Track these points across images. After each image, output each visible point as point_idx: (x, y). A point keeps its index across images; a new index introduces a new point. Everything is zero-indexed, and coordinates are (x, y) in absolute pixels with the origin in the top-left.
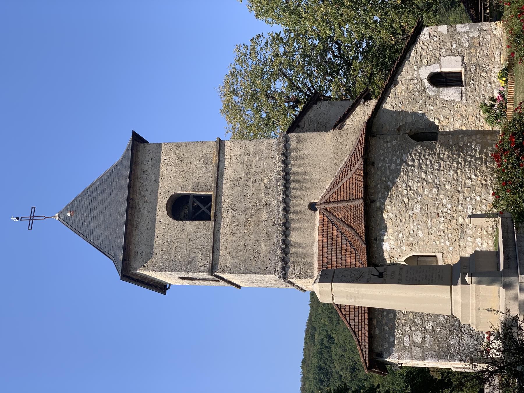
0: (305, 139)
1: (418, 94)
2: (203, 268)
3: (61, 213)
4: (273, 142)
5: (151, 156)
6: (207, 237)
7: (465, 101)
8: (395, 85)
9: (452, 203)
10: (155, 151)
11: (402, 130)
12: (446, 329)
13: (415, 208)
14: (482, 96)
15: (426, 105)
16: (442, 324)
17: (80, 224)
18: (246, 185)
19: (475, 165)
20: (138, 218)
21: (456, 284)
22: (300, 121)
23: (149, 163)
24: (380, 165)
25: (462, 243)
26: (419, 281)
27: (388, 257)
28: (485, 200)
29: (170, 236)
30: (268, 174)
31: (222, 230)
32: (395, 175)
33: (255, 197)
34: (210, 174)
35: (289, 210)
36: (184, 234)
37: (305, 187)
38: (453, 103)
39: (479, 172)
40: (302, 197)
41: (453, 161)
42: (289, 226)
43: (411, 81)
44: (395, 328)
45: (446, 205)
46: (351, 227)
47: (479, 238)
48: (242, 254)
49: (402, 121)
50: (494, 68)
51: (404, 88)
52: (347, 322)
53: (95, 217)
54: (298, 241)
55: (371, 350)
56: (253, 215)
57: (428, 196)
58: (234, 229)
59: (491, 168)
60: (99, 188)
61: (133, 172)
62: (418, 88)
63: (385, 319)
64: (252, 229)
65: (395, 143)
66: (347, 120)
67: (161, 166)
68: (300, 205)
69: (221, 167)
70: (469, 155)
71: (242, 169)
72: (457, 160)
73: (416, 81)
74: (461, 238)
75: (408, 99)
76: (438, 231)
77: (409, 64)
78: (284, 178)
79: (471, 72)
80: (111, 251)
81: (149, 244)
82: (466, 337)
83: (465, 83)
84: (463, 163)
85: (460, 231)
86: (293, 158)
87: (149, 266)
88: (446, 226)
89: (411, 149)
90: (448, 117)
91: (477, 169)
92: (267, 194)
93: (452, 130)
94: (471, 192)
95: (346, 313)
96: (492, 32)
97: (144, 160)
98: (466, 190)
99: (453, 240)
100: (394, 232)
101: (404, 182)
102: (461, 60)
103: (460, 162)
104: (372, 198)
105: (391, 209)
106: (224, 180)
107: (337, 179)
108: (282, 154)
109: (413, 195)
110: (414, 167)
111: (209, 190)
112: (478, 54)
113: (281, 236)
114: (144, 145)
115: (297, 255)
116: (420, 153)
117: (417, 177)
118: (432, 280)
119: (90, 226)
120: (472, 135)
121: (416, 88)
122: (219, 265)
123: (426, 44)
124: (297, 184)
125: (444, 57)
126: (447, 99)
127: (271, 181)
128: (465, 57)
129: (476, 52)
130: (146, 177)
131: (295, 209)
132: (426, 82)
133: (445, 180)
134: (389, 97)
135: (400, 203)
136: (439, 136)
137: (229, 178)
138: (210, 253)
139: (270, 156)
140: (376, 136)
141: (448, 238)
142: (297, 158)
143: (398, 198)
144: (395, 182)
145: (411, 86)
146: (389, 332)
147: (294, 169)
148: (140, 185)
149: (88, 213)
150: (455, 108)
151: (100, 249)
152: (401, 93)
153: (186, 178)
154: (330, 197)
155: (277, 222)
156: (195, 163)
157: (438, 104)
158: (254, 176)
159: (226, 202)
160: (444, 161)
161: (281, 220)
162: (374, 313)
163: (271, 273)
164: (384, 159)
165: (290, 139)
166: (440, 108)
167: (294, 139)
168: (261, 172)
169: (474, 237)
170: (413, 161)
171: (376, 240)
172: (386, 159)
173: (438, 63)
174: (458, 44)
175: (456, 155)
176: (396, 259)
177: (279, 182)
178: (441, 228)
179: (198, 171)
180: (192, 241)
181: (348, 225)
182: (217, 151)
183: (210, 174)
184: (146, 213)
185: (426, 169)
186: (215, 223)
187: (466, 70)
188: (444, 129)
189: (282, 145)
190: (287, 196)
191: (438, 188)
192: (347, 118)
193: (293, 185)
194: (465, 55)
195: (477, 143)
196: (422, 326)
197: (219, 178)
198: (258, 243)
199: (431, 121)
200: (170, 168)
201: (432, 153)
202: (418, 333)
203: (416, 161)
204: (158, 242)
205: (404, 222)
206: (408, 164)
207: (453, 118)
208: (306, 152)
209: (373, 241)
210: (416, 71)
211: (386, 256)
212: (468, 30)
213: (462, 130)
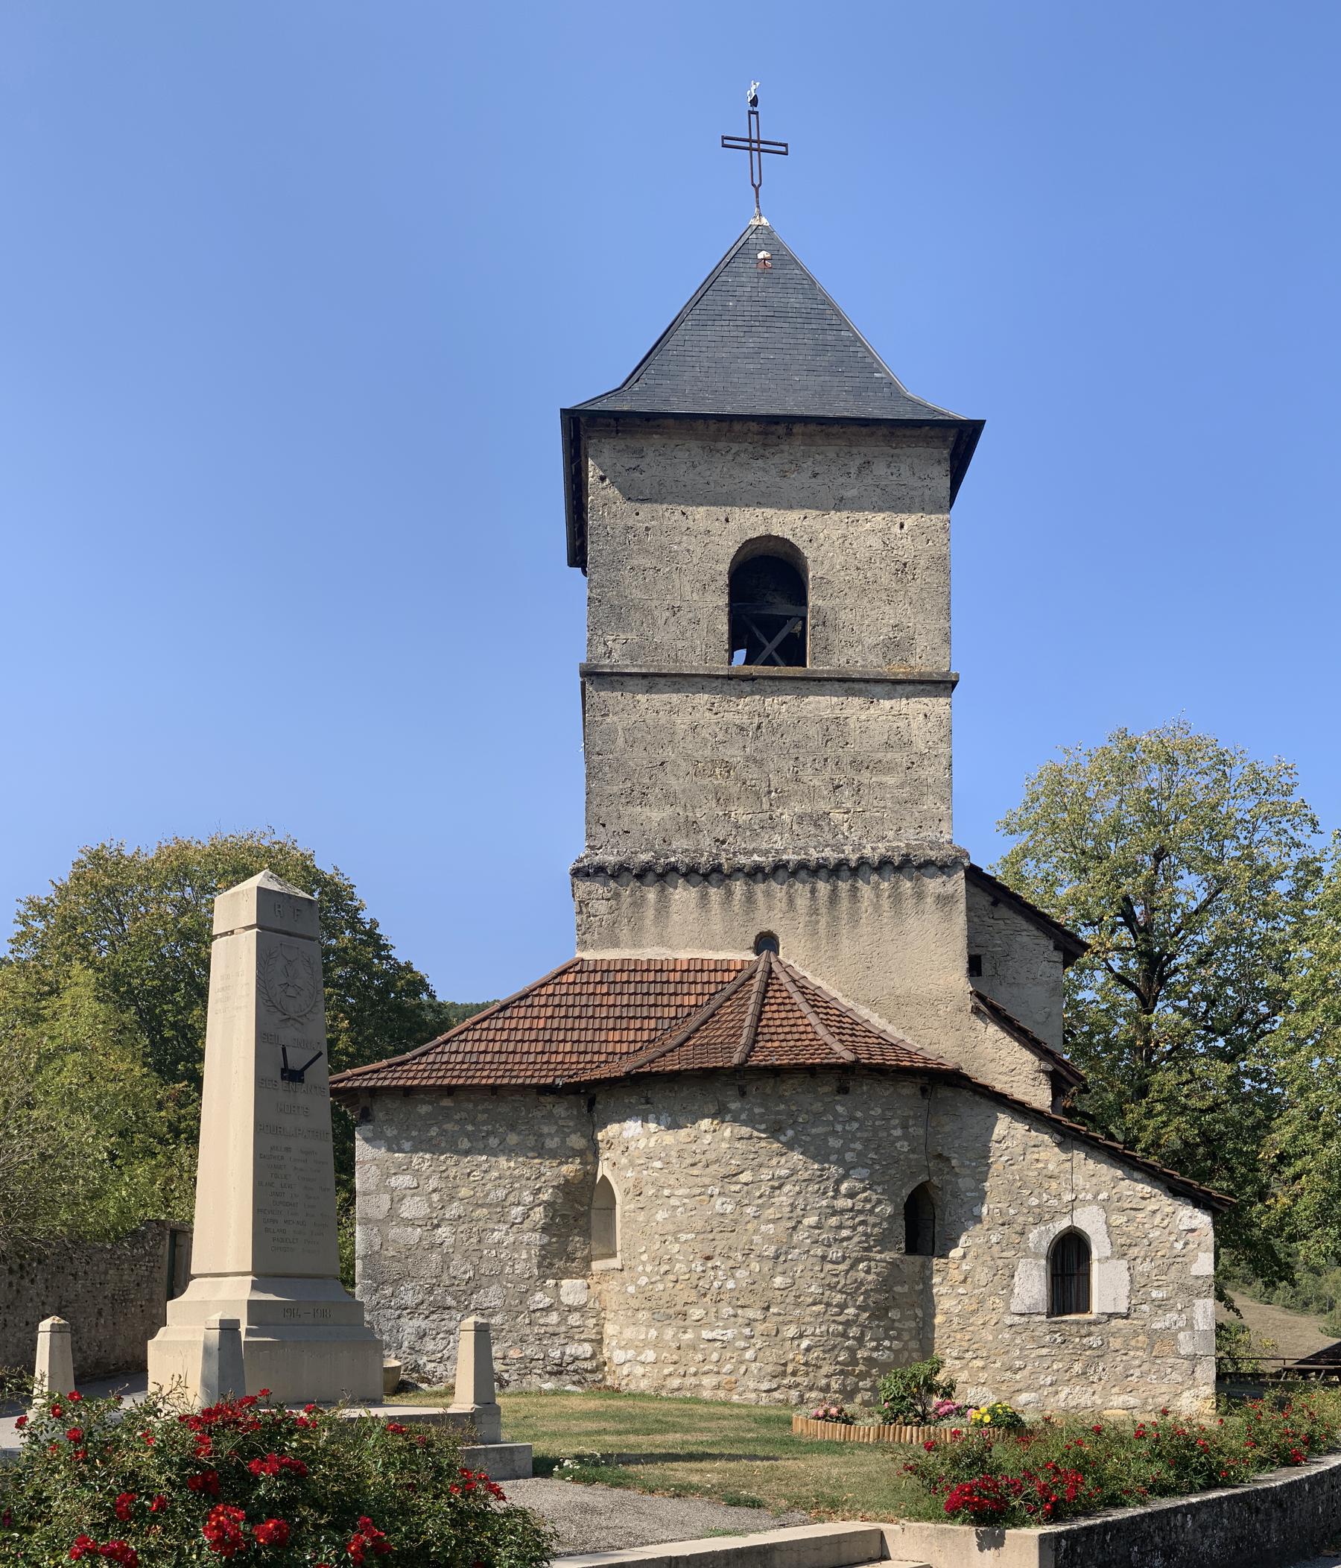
0: (948, 918)
1: (1034, 1204)
2: (601, 649)
3: (769, 231)
5: (914, 482)
6: (683, 658)
7: (1009, 1322)
8: (1059, 1145)
9: (737, 1291)
10: (927, 492)
12: (436, 1277)
15: (1003, 1225)
17: (731, 289)
18: (826, 760)
19: (834, 1347)
20: (737, 454)
21: (255, 1286)
22: (1010, 907)
23: (894, 478)
24: (840, 1109)
25: (644, 1315)
26: (271, 1185)
27: (611, 1134)
29: (688, 551)
31: (703, 698)
32: (812, 1148)
33: (793, 786)
34: (859, 659)
35: (755, 881)
36: (692, 592)
37: (817, 922)
39: (817, 1358)
40: (792, 914)
41: (848, 1294)
42: (714, 882)
44: (434, 1154)
45: (733, 1277)
46: (688, 1039)
48: (637, 758)
49: (962, 1165)
50: (1094, 1393)
51: (1051, 1167)
52: (455, 1036)
53: (746, 329)
54: (674, 908)
55: (373, 1092)
56: (744, 783)
57: (756, 1231)
58: (705, 733)
59: (828, 1385)
60: (830, 337)
61: (864, 430)
62: (1048, 1204)
63: (456, 1128)
64: (706, 781)
66: (996, 1028)
67: (883, 515)
68: (770, 908)
69: (878, 689)
70: (863, 1334)
71: (870, 749)
72: (850, 1303)
73: (1068, 1197)
75: (1020, 1180)
77: (1115, 1179)
78: (842, 864)
80: (648, 381)
81: (664, 490)
82: (419, 1322)
83: (1056, 1323)
84: (840, 1318)
85: (671, 1311)
86: (895, 887)
87: (603, 493)
88: (681, 1278)
89: (884, 1189)
90: (969, 1280)
91: (824, 1351)
92: (801, 818)
93: (935, 1291)
94: (764, 1338)
95: (478, 1033)
96: (1189, 1389)
97: (901, 462)
98: (770, 1326)
99: (651, 1293)
100: (665, 1148)
101: (794, 1172)
102: (1117, 1311)
104: (752, 1089)
105: (723, 1140)
106: (841, 699)
107: (826, 1002)
108: (908, 855)
109: (758, 1194)
110: (834, 1198)
112: (1132, 1353)
113: (687, 860)
114: (945, 459)
115: (638, 904)
116: (871, 1211)
117: (806, 1206)
118: (274, 1221)
119: (723, 318)
120: (920, 1341)
122: (610, 694)
123: (1166, 1222)
124: (825, 898)
126: (1016, 1278)
127: (835, 831)
128: (1124, 1321)
129: (1137, 1349)
130: (852, 471)
131: (760, 896)
132: (1064, 1224)
133: (798, 1274)
134: (1029, 1130)
136: (918, 1259)
137: (847, 712)
138: (641, 666)
140: (924, 1098)
141: (655, 1282)
142: (897, 898)
143: (751, 1156)
144: (792, 1150)
145: (1054, 1185)
146: (423, 1138)
147: (866, 891)
148: (832, 455)
149: (760, 309)
150: (992, 1298)
151: (656, 350)
152: (1037, 1160)
154: (781, 985)
155: (724, 850)
156: (890, 615)
157: (1004, 1254)
158: (850, 783)
159: (781, 706)
160: (847, 1272)
161: (727, 859)
162: (469, 1100)
163: (589, 836)
164: (856, 1119)
165: (949, 876)
166: (993, 1260)
167: (949, 889)
168: (862, 803)
169: (657, 1344)
170: (851, 1195)
171: (647, 1103)
172: (856, 1125)
175: (864, 1301)
176: (607, 1155)
177: (833, 851)
178: (678, 1266)
179: (866, 622)
180: (674, 614)
181: (697, 1030)
182: (920, 674)
183: (859, 659)
184: (750, 477)
185: (827, 1227)
186: (723, 677)
187: (1090, 1323)
188: (938, 1271)
189: (933, 854)
190: (794, 874)
191: (777, 1257)
192: (1002, 1028)
193: (823, 887)
194: (1130, 1321)
195: (897, 1353)
196: (443, 1219)
197: (846, 685)
198: (669, 798)
199: (959, 1238)
200: (875, 542)
201: (872, 1243)
202: (425, 1210)
203: (849, 1203)
204: (668, 515)
206: (842, 1183)
207: (965, 1292)
208: (912, 923)
209: (644, 1095)
210: (1095, 1197)
211: (613, 1129)
212: (1196, 1328)
213: (934, 1316)
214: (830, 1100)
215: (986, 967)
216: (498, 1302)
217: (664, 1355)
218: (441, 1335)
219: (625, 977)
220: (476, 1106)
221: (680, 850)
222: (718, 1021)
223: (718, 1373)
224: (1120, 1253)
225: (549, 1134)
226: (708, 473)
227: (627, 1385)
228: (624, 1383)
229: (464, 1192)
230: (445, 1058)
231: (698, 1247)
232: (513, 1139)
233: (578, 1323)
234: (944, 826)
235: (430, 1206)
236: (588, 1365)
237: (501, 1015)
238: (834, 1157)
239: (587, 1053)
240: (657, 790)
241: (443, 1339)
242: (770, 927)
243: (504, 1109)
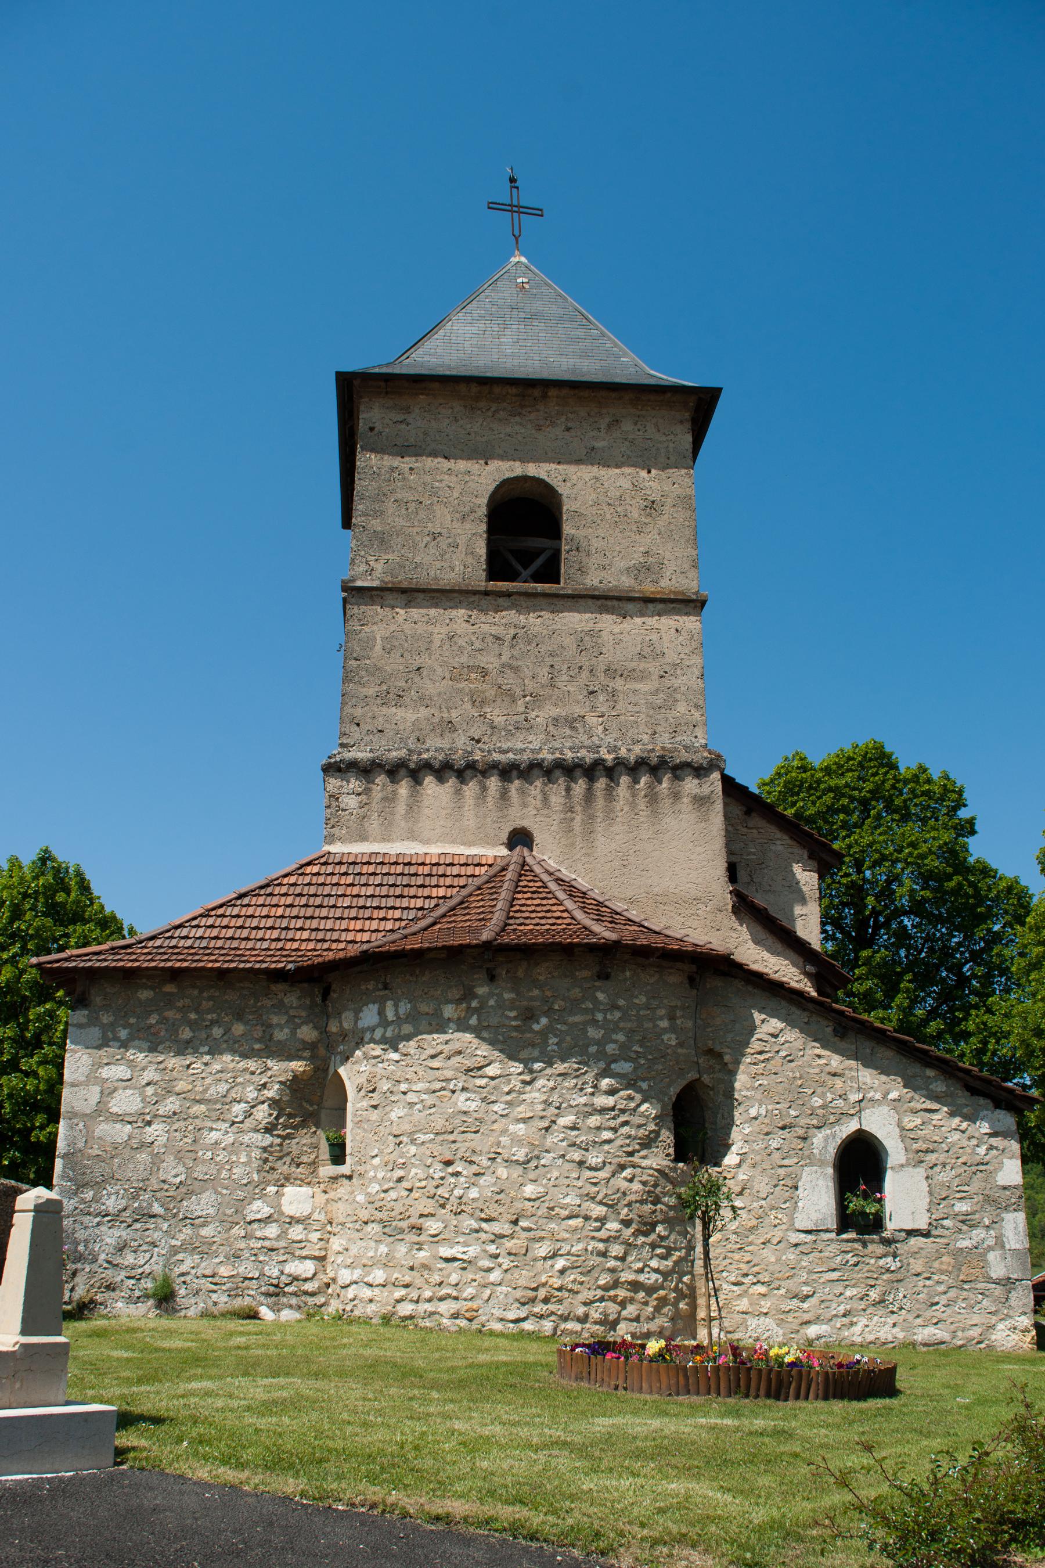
1: (817, 1104)
4: (699, 735)
7: (794, 1241)
9: (481, 1202)
10: (671, 445)
11: (712, 1062)
13: (469, 1095)
14: (809, 1289)
15: (783, 1128)
16: (159, 1169)
23: (641, 433)
24: (601, 996)
25: (374, 1228)
28: (489, 1298)
30: (610, 723)
32: (568, 1038)
37: (573, 819)
38: (787, 1205)
39: (574, 1281)
40: (546, 812)
43: (854, 1084)
47: (385, 1276)
48: (394, 664)
50: (894, 1325)
61: (614, 395)
63: (178, 1016)
65: (669, 1039)
69: (630, 606)
71: (624, 659)
73: (854, 1097)
74: (385, 1227)
76: (404, 1164)
78: (598, 763)
79: (880, 1258)
89: (649, 1086)
92: (556, 721)
94: (512, 1258)
99: (381, 1203)
103: (607, 1226)
108: (663, 757)
109: (506, 1089)
111: (565, 583)
112: (936, 1277)
115: (390, 800)
121: (834, 1100)
125: (927, 1178)
126: (800, 1190)
129: (942, 1272)
130: (603, 427)
132: (852, 1126)
135: (485, 1054)
137: (598, 627)
139: (659, 729)
142: (653, 798)
145: (838, 1082)
146: (142, 1025)
153: (599, 522)
156: (644, 542)
159: (536, 621)
162: (194, 987)
167: (706, 790)
172: (618, 1014)
173: (908, 1159)
174: (965, 1217)
178: (414, 1171)
180: (434, 539)
184: (508, 430)
194: (932, 1239)
196: (156, 1116)
197: (599, 602)
198: (423, 700)
205: (431, 1065)
208: (670, 822)
210: (885, 1096)
212: (1007, 1247)
214: (588, 985)
215: (742, 875)
216: (211, 1211)
217: (396, 1275)
218: (145, 1247)
219: (371, 869)
220: (201, 992)
221: (435, 747)
222: (467, 908)
223: (456, 1298)
224: (918, 1158)
225: (278, 1025)
226: (469, 426)
227: (352, 1311)
228: (348, 1308)
229: (181, 1086)
230: (174, 942)
231: (437, 1149)
232: (239, 1029)
233: (299, 1238)
234: (699, 732)
235: (143, 1101)
236: (309, 1287)
237: (239, 902)
238: (593, 1049)
239: (326, 941)
240: (413, 693)
241: (145, 1251)
242: (526, 823)
243: (231, 996)
